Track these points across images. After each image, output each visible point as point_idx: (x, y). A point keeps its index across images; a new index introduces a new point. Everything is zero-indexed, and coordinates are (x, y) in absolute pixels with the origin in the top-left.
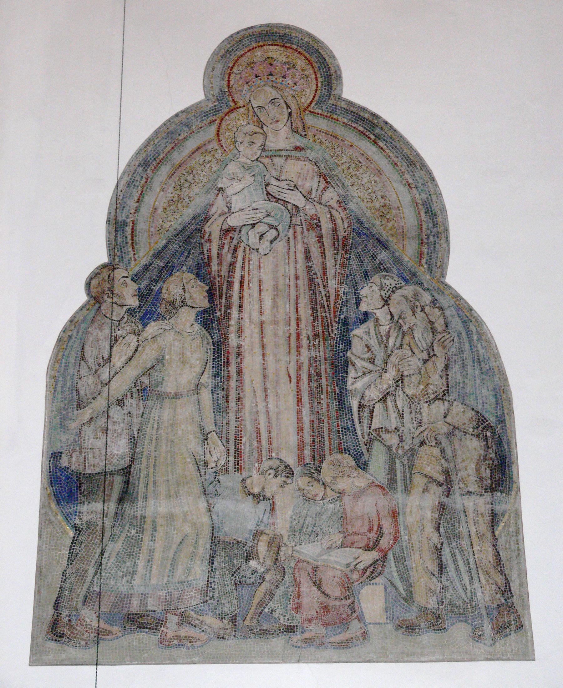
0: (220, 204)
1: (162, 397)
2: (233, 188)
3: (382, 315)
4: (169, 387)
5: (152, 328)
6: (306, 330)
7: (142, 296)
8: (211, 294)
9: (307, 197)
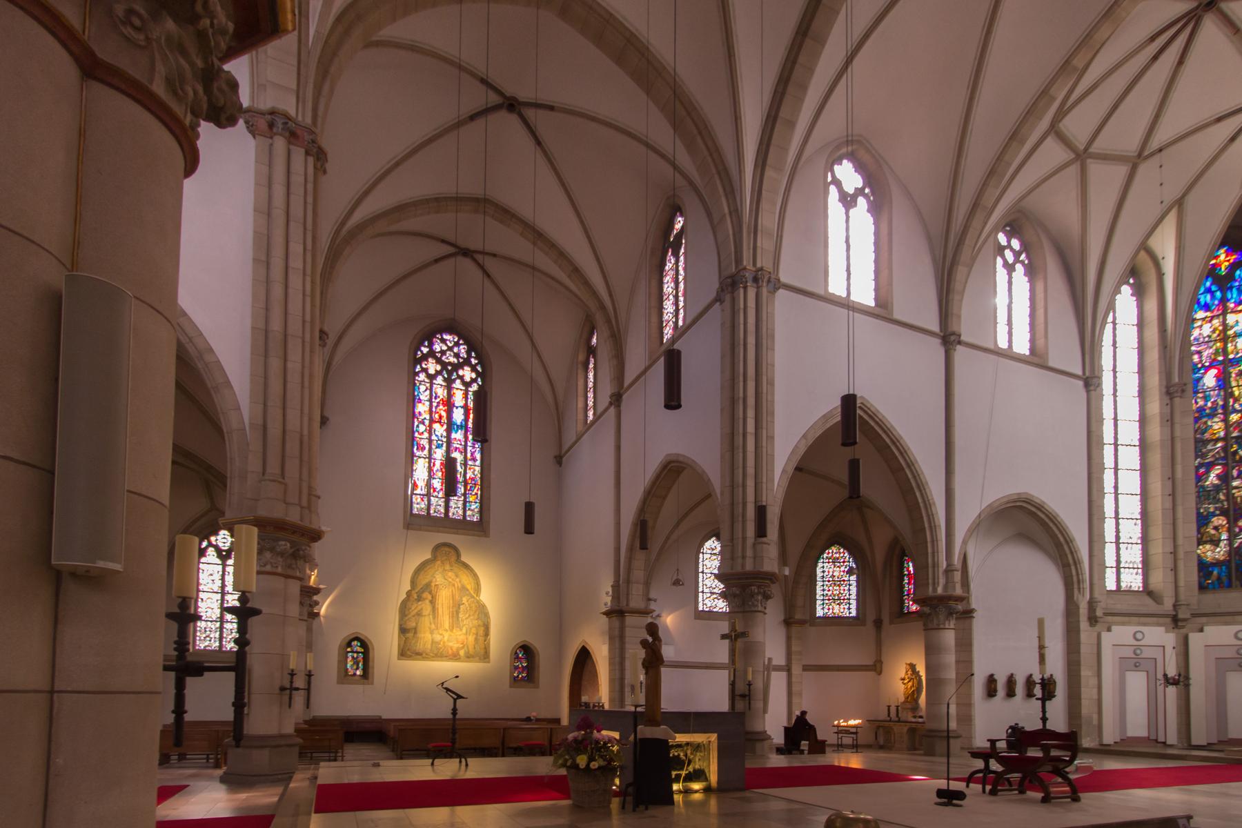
0: (434, 580)
1: (422, 616)
2: (437, 577)
3: (466, 603)
4: (424, 614)
5: (420, 603)
6: (451, 605)
7: (418, 596)
8: (432, 597)
9: (453, 580)
